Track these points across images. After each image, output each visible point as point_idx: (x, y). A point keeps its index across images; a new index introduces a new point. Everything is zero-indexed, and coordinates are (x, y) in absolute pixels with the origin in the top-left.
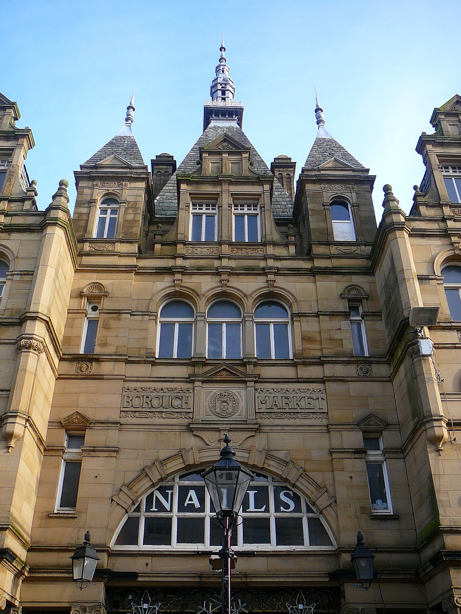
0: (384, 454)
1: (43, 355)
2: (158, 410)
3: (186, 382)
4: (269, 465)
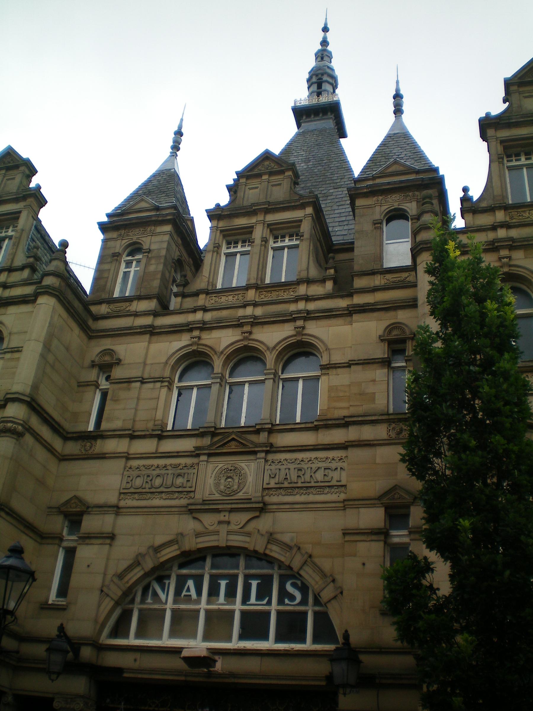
1: (28, 439)
2: (158, 490)
3: (191, 456)
4: (271, 550)
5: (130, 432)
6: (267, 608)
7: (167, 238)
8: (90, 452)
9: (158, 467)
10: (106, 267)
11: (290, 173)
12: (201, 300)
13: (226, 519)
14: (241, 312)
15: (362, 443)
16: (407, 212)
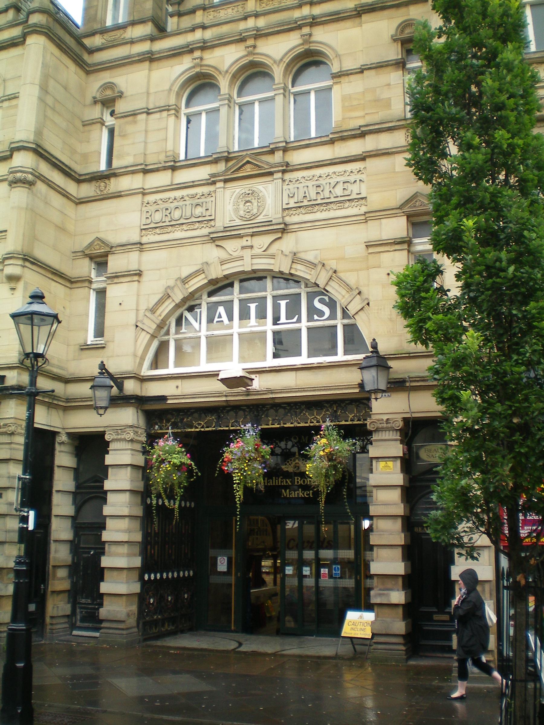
1: (40, 186)
3: (208, 184)
4: (296, 270)
5: (143, 167)
8: (105, 192)
9: (175, 199)
13: (249, 243)
14: (242, 26)
15: (380, 152)
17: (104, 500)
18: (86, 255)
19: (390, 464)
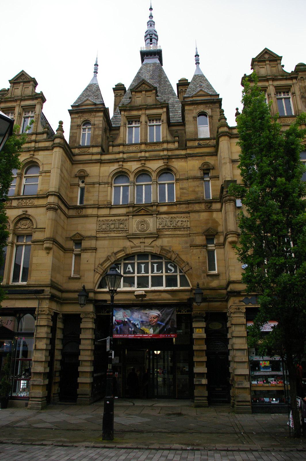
0: (215, 246)
1: (59, 211)
5: (98, 206)
6: (161, 274)
7: (102, 119)
8: (81, 214)
10: (75, 131)
11: (154, 91)
12: (121, 148)
13: (143, 241)
14: (139, 155)
16: (207, 113)
17: (79, 343)
18: (72, 240)
19: (201, 330)
